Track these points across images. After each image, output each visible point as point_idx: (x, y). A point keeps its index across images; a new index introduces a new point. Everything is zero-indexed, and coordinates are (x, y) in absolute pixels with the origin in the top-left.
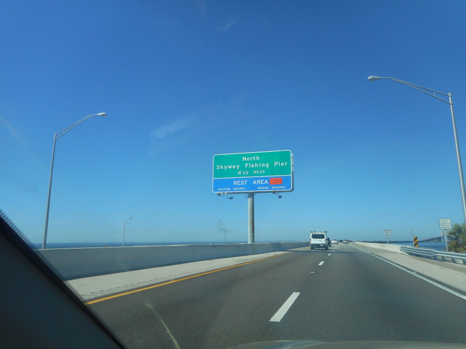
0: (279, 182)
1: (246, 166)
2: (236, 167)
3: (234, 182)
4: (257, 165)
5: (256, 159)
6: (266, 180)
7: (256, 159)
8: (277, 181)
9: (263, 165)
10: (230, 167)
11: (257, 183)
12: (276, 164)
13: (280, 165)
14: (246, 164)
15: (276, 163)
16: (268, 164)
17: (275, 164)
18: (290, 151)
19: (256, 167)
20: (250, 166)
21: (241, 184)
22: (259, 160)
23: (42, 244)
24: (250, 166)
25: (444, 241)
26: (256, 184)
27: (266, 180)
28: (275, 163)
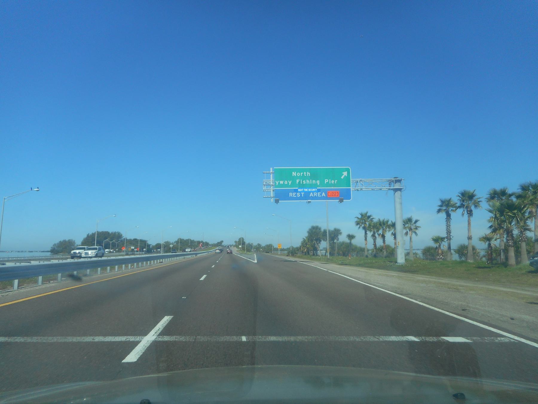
0: (336, 195)
1: (297, 182)
2: (288, 182)
3: (290, 193)
4: (308, 182)
5: (306, 174)
6: (323, 193)
7: (306, 174)
8: (335, 193)
9: (314, 182)
11: (313, 195)
12: (327, 181)
13: (331, 182)
14: (297, 180)
15: (327, 181)
16: (319, 181)
17: (326, 182)
18: (349, 168)
19: (307, 183)
20: (301, 182)
21: (298, 196)
22: (310, 175)
24: (301, 182)
26: (313, 196)
27: (323, 193)
28: (326, 180)
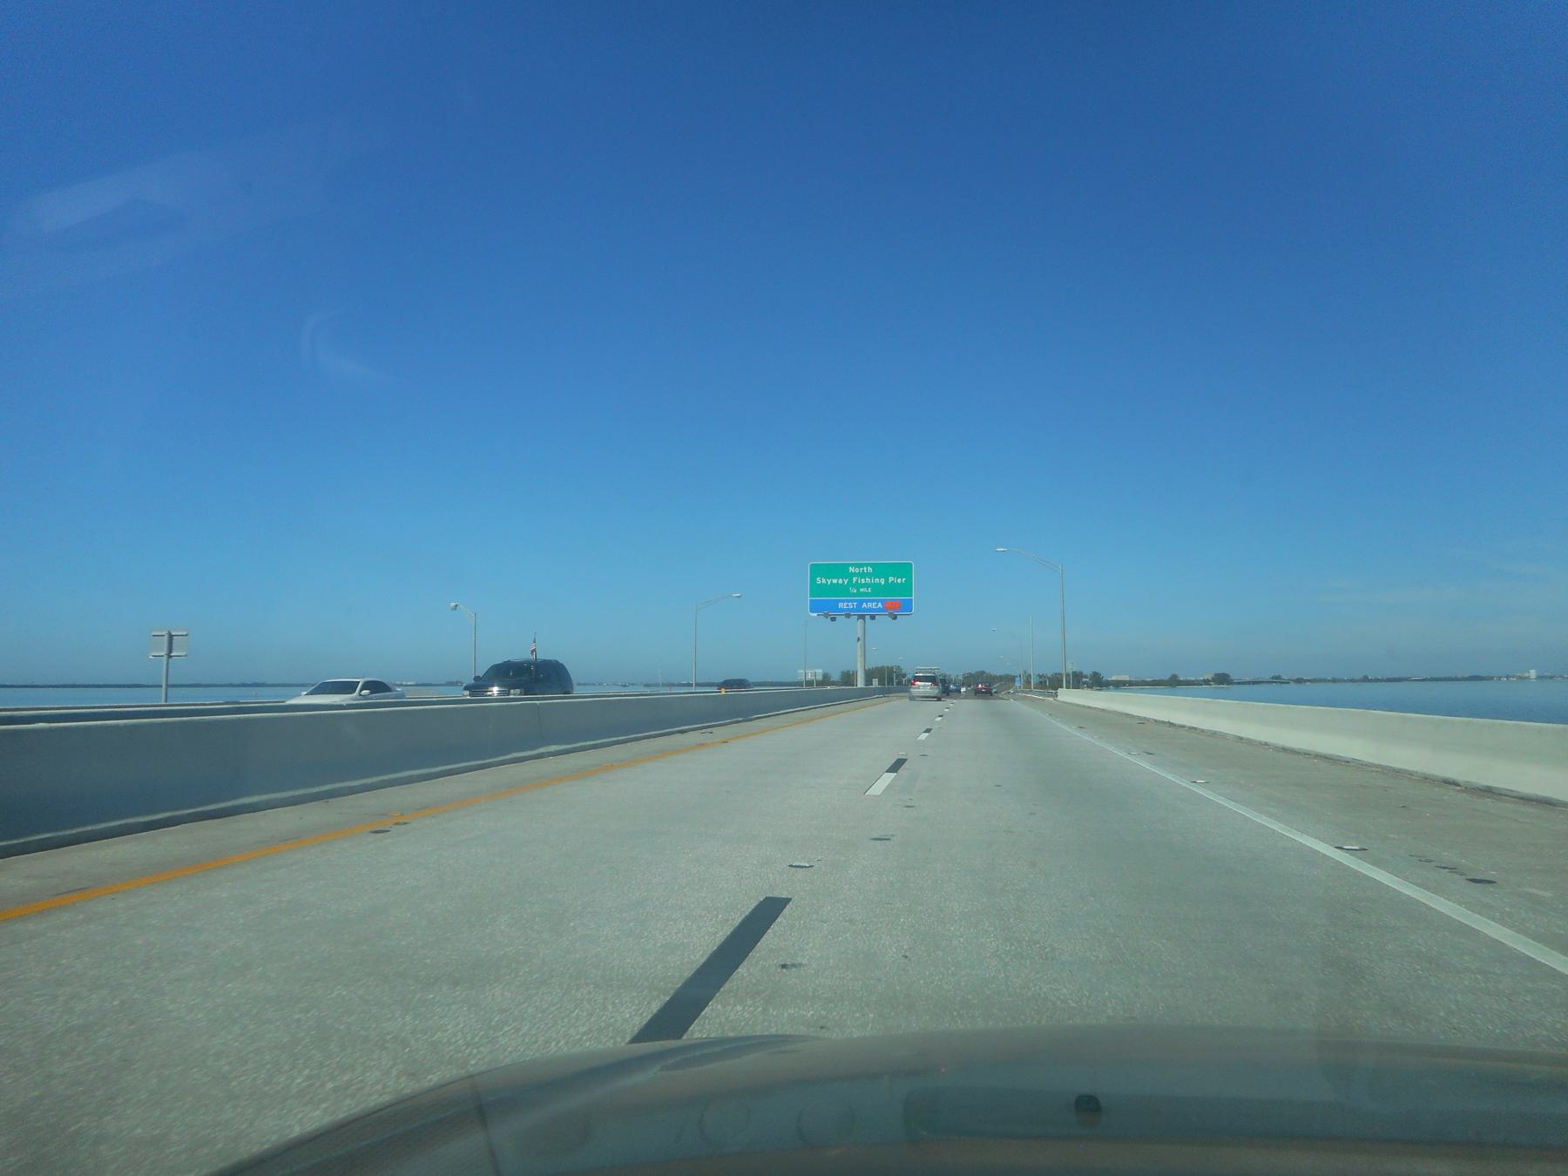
10: (835, 581)
23: (1061, 675)
25: (1459, 785)
